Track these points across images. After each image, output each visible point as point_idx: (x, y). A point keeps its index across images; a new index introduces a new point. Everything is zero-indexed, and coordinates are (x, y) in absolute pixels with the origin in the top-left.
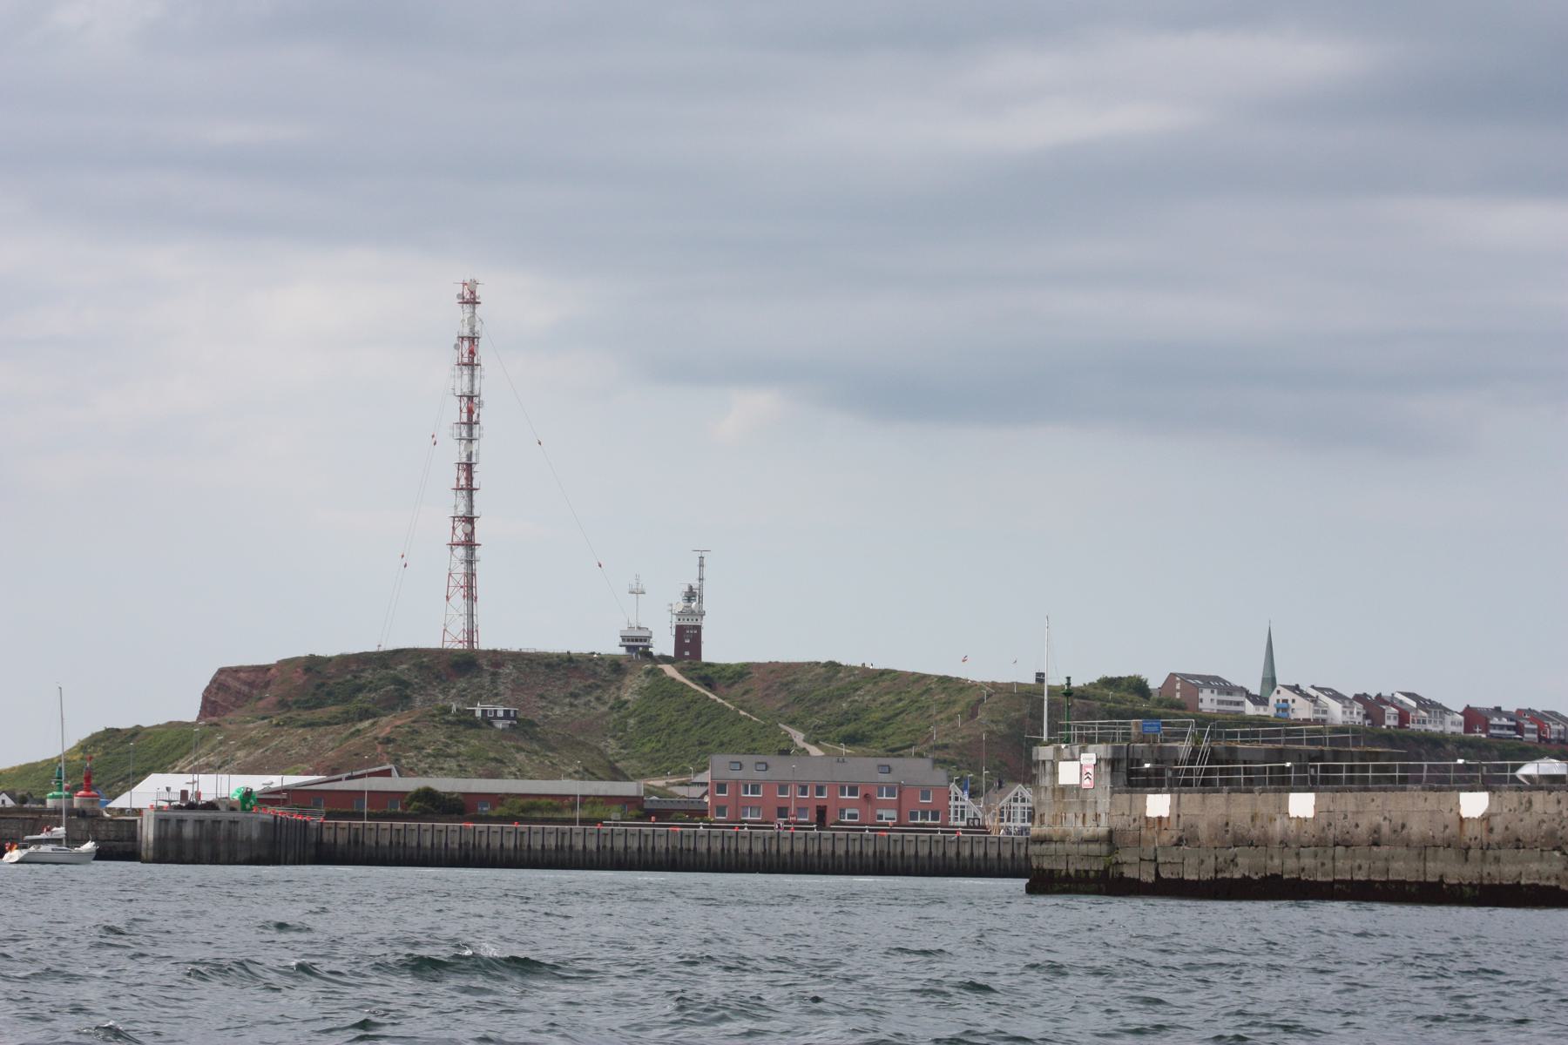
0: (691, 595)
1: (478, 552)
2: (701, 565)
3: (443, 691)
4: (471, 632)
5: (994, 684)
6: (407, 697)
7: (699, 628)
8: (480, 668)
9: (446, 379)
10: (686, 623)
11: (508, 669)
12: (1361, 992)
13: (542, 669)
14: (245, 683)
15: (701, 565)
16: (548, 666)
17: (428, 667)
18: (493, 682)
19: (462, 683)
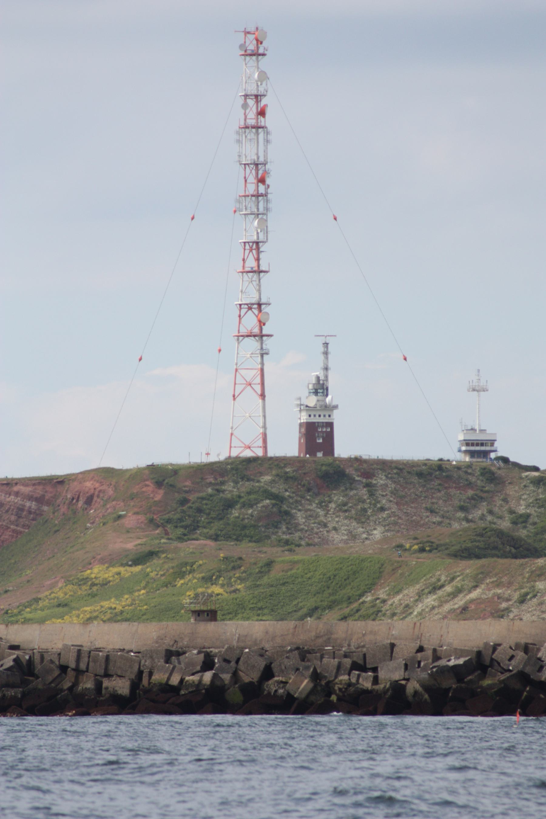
0: (320, 388)
1: (330, 356)
2: (326, 353)
3: (320, 505)
4: (261, 447)
5: (107, 473)
6: (287, 513)
7: (330, 425)
8: (352, 481)
9: (280, 155)
10: (317, 420)
11: (380, 480)
12: (130, 746)
13: (415, 479)
14: (30, 498)
15: (326, 353)
16: (420, 475)
17: (294, 479)
18: (371, 494)
19: (338, 497)
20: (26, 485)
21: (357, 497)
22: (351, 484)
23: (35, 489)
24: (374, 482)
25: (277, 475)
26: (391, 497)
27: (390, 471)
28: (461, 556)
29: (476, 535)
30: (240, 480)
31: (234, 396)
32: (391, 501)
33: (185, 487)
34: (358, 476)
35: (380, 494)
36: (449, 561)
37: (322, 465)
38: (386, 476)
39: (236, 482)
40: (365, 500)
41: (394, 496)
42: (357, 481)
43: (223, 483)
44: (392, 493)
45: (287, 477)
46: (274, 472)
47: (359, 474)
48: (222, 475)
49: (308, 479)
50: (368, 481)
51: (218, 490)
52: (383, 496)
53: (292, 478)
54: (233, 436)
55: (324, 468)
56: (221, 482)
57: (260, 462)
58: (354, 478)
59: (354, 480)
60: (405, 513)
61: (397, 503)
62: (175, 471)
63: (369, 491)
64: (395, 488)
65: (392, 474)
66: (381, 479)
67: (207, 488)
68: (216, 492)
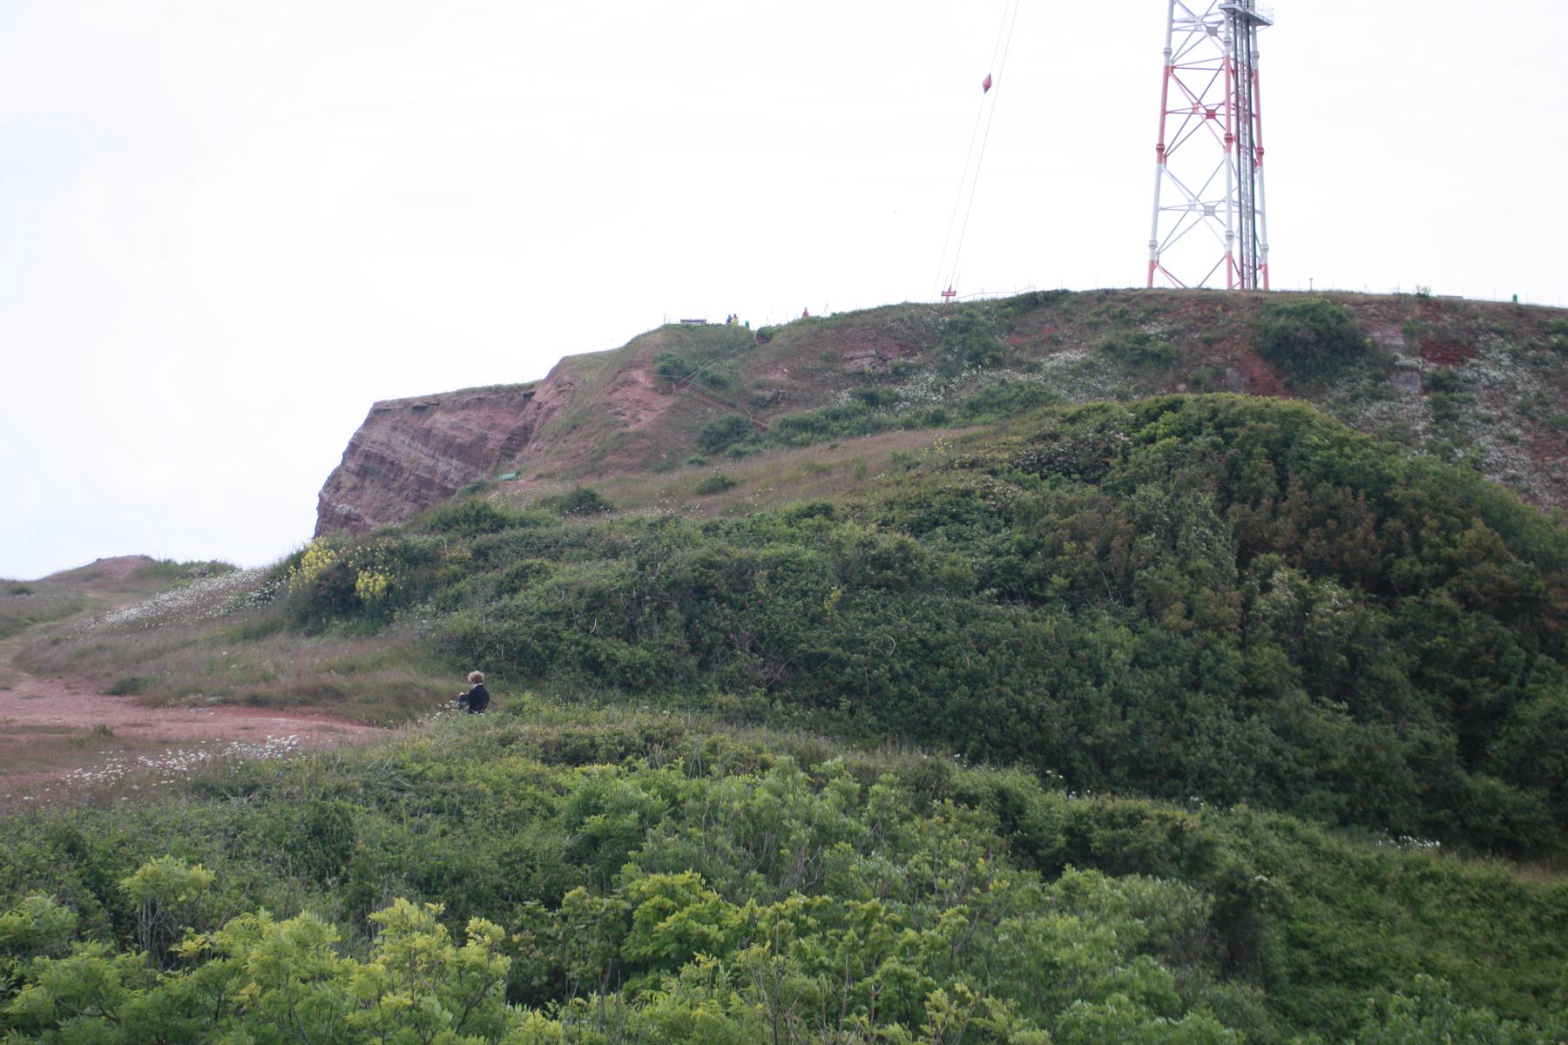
18: (1443, 415)
20: (450, 411)
21: (1389, 424)
22: (1378, 378)
23: (465, 419)
24: (1468, 374)
25: (1110, 348)
26: (1518, 425)
27: (1534, 339)
28: (593, 666)
29: (1044, 465)
30: (966, 364)
31: (1160, 148)
32: (1512, 440)
33: (759, 387)
34: (1409, 352)
35: (1477, 416)
36: (99, 699)
37: (1278, 314)
38: (1515, 355)
39: (948, 371)
40: (1416, 434)
41: (1527, 423)
42: (1404, 368)
43: (900, 375)
44: (1523, 410)
45: (1145, 354)
46: (1103, 339)
47: (1417, 344)
48: (907, 348)
49: (1216, 359)
50: (1442, 373)
51: (872, 400)
52: (1488, 421)
53: (1157, 356)
54: (1156, 271)
55: (1282, 321)
56: (896, 371)
57: (1065, 305)
58: (1396, 359)
59: (1392, 367)
60: (1557, 481)
61: (1533, 449)
62: (730, 341)
63: (1437, 405)
64: (1539, 395)
65: (1540, 349)
66: (1496, 363)
67: (839, 389)
68: (861, 405)
